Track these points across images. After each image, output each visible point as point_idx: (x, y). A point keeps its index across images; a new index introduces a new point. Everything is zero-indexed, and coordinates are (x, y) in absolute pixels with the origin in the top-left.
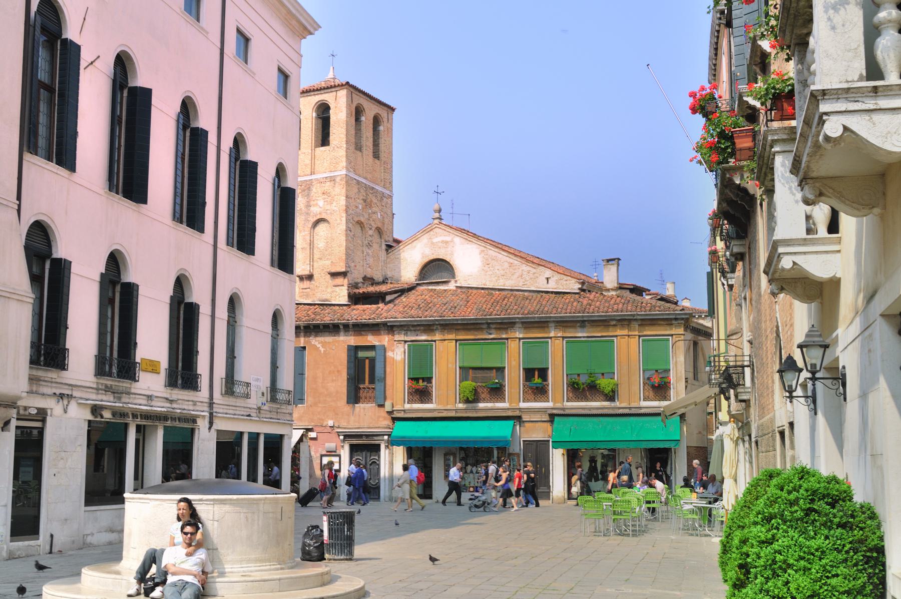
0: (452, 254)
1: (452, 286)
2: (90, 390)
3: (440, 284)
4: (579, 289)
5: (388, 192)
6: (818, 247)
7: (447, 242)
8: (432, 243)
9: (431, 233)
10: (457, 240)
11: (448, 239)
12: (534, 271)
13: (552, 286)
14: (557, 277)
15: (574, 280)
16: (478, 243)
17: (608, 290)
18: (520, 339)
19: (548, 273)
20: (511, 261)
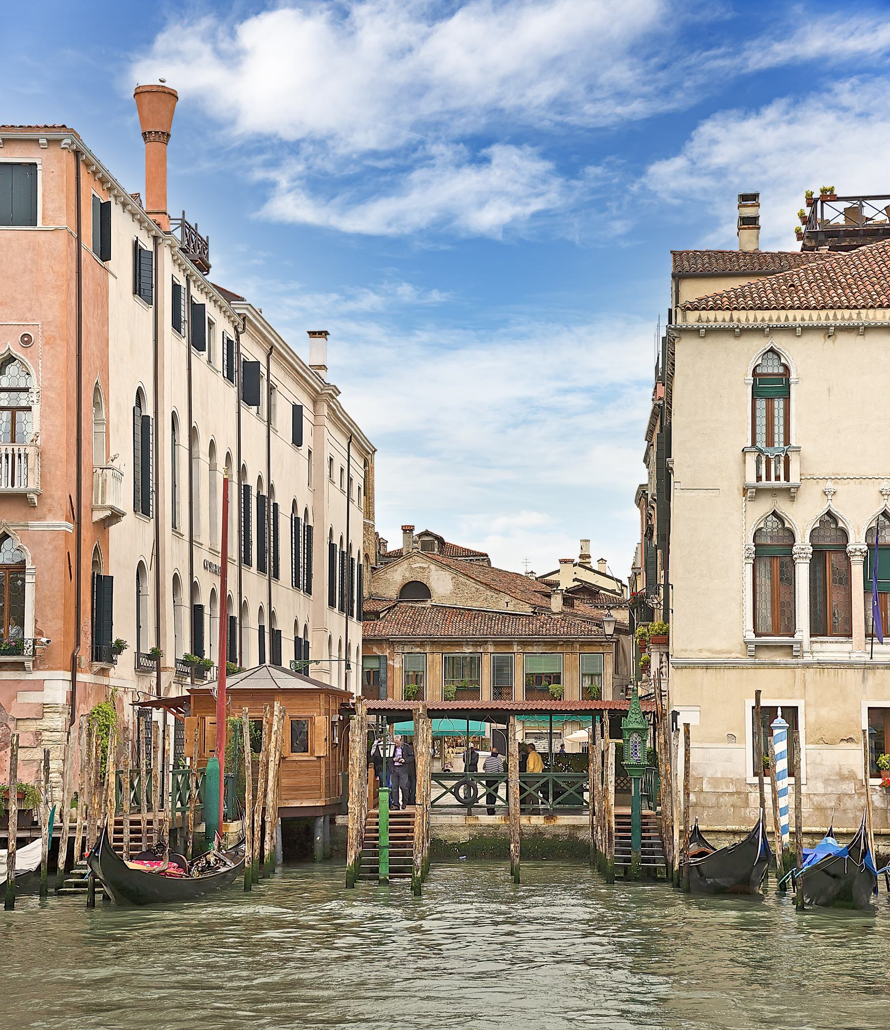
0: (428, 578)
1: (428, 604)
2: (309, 389)
3: (229, 499)
4: (532, 612)
5: (372, 522)
6: (201, 502)
7: (424, 568)
8: (411, 568)
9: (411, 559)
10: (433, 567)
11: (425, 566)
12: (497, 596)
13: (510, 609)
14: (515, 602)
15: (528, 605)
16: (724, 656)
17: (555, 614)
18: (491, 653)
19: (507, 598)
20: (478, 587)
